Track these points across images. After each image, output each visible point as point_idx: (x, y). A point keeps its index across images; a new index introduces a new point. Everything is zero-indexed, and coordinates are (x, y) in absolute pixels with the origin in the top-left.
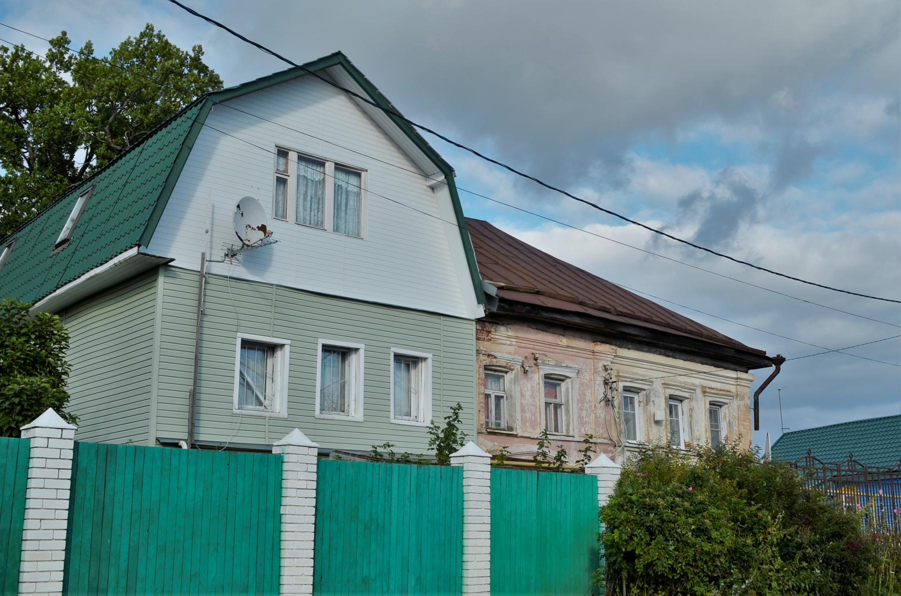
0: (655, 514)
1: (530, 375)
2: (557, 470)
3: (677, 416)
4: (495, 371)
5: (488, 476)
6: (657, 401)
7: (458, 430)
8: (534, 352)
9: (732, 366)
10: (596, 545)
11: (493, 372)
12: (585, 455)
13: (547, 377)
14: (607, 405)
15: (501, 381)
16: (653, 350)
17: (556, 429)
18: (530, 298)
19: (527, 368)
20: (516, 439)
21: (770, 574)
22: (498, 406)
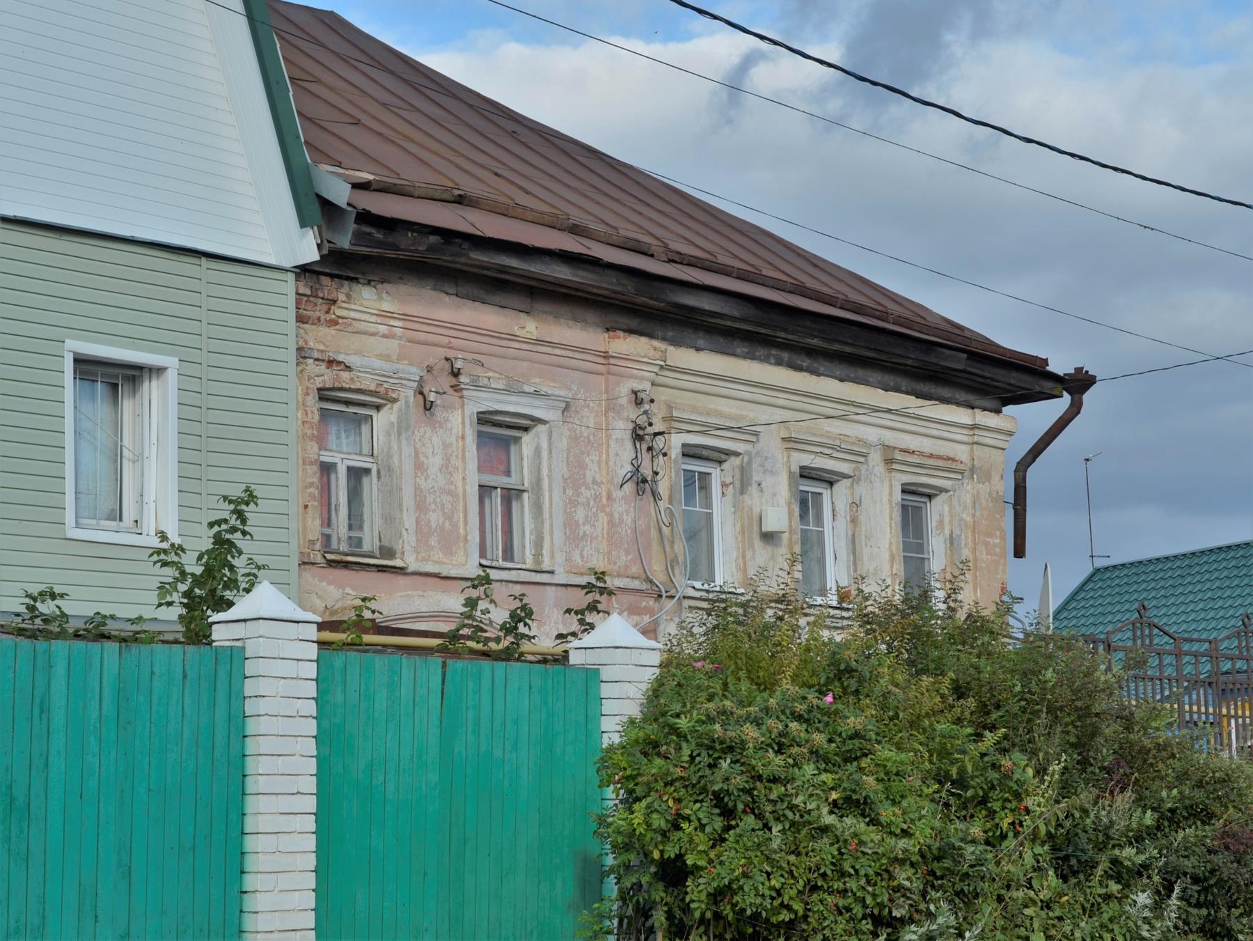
0: (1140, 801)
1: (439, 413)
2: (507, 655)
3: (819, 520)
4: (348, 403)
5: (311, 670)
6: (768, 482)
7: (240, 553)
8: (451, 354)
9: (962, 396)
10: (594, 846)
11: (343, 404)
12: (581, 622)
13: (485, 419)
14: (639, 492)
15: (365, 429)
16: (761, 351)
17: (508, 553)
18: (440, 219)
19: (432, 397)
20: (401, 580)
21: (1028, 912)
22: (355, 495)
